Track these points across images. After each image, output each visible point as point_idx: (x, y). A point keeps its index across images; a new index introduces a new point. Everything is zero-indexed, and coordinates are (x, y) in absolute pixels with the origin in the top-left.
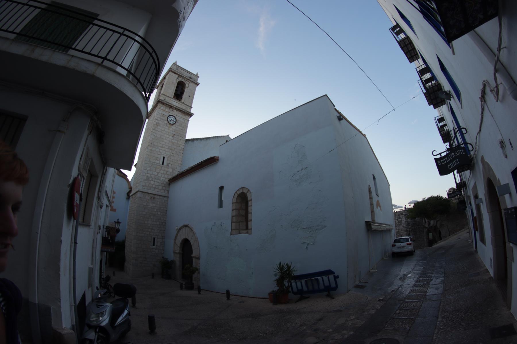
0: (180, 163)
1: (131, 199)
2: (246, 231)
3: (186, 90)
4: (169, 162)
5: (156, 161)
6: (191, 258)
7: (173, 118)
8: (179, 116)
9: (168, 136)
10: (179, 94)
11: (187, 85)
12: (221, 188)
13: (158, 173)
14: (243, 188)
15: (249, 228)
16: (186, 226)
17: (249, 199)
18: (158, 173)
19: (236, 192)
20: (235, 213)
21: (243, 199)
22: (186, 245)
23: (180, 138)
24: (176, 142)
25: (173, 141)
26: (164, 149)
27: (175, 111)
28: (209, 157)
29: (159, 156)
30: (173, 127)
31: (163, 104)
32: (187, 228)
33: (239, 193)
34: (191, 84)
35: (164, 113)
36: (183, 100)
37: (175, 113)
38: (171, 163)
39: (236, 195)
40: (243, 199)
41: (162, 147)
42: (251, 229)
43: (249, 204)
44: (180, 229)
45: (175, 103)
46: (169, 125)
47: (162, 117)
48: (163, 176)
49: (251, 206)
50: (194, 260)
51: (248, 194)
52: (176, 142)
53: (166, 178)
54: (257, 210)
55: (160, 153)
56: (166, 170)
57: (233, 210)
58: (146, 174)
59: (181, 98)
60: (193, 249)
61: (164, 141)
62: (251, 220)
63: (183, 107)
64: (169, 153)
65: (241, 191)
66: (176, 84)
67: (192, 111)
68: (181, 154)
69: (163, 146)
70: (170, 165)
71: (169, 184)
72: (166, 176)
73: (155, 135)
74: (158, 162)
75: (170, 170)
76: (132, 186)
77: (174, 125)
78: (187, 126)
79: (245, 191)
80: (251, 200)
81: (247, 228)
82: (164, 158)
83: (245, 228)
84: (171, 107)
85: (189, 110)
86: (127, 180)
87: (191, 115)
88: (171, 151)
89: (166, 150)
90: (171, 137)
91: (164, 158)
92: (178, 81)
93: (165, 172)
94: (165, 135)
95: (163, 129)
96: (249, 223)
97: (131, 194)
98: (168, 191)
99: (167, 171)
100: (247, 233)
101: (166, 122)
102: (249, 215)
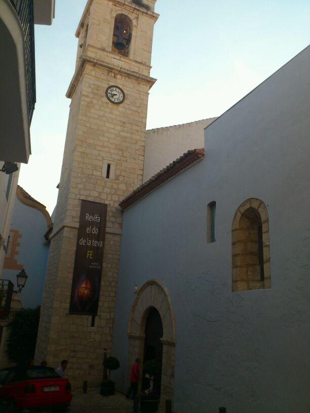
0: (141, 172)
1: (52, 243)
2: (259, 284)
3: (134, 33)
4: (118, 173)
5: (95, 173)
6: (161, 344)
7: (115, 92)
8: (128, 86)
9: (112, 126)
10: (122, 43)
11: (134, 22)
12: (212, 205)
13: (100, 193)
14: (250, 200)
15: (266, 275)
16: (151, 283)
17: (263, 218)
18: (100, 193)
19: (238, 209)
20: (239, 249)
21: (252, 219)
22: (152, 318)
23: (135, 128)
24: (129, 135)
25: (122, 134)
26: (107, 149)
27: (119, 77)
28: (186, 152)
29: (100, 164)
30: (121, 108)
31: (95, 65)
32: (154, 286)
33: (243, 210)
34: (143, 19)
35: (99, 84)
36: (131, 56)
37: (120, 81)
38: (123, 174)
39: (239, 215)
40: (252, 219)
41: (103, 147)
42: (270, 278)
43: (264, 230)
44: (142, 290)
45: (116, 61)
46: (111, 105)
47: (95, 91)
48: (109, 198)
49: (267, 232)
50: (165, 348)
51: (260, 210)
52: (129, 135)
53: (115, 202)
54: (277, 241)
55: (101, 158)
56: (115, 186)
57: (233, 244)
58: (78, 197)
59: (128, 53)
60: (164, 326)
61: (106, 135)
62: (269, 260)
63: (135, 68)
64: (117, 157)
65: (248, 206)
66: (113, 21)
67: (152, 75)
68: (141, 158)
69: (106, 144)
70: (121, 178)
71: (122, 212)
72: (116, 198)
73: (88, 125)
74: (98, 173)
75: (123, 187)
76: (53, 222)
77: (121, 105)
78: (147, 105)
79: (255, 205)
80: (267, 221)
81: (262, 278)
82: (109, 166)
83: (259, 278)
84: (110, 70)
85: (145, 74)
86: (46, 213)
87: (151, 82)
88: (120, 153)
89: (112, 151)
90: (119, 128)
91: (109, 166)
92: (114, 15)
93: (113, 192)
94: (107, 124)
95: (101, 113)
96: (265, 266)
97: (51, 235)
98: (121, 225)
99: (116, 190)
100: (263, 287)
101: (105, 99)
102: (265, 249)
